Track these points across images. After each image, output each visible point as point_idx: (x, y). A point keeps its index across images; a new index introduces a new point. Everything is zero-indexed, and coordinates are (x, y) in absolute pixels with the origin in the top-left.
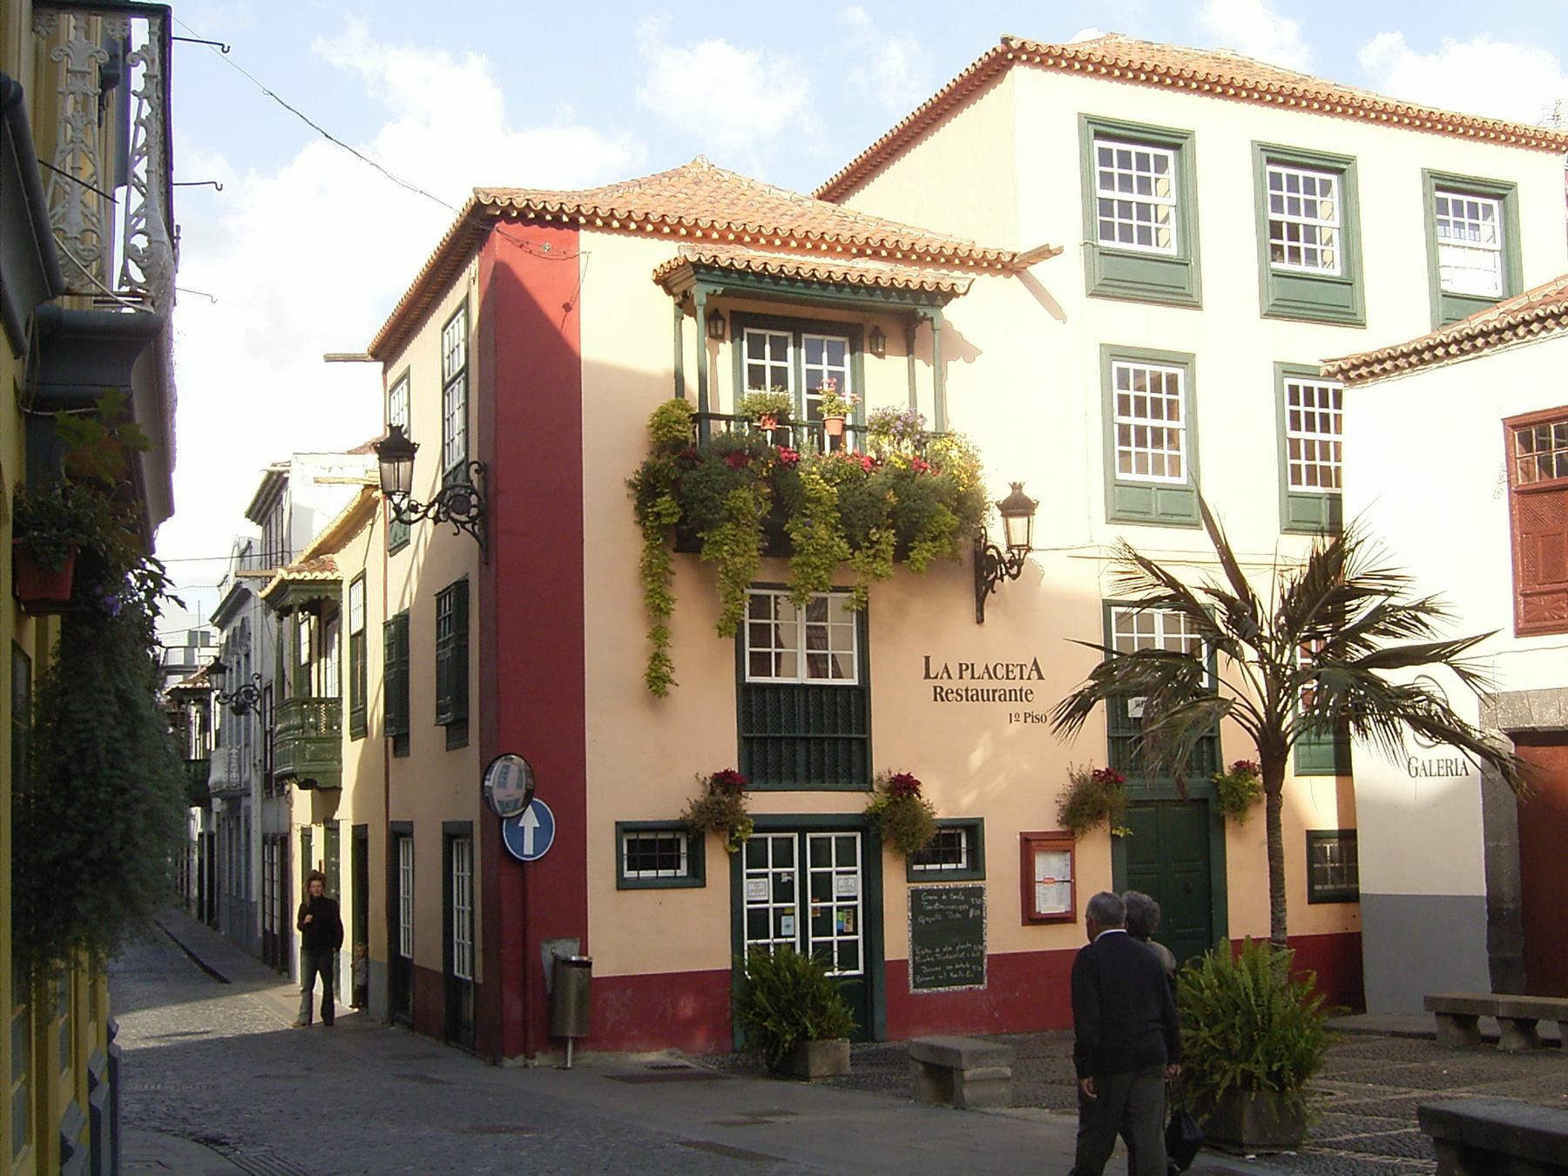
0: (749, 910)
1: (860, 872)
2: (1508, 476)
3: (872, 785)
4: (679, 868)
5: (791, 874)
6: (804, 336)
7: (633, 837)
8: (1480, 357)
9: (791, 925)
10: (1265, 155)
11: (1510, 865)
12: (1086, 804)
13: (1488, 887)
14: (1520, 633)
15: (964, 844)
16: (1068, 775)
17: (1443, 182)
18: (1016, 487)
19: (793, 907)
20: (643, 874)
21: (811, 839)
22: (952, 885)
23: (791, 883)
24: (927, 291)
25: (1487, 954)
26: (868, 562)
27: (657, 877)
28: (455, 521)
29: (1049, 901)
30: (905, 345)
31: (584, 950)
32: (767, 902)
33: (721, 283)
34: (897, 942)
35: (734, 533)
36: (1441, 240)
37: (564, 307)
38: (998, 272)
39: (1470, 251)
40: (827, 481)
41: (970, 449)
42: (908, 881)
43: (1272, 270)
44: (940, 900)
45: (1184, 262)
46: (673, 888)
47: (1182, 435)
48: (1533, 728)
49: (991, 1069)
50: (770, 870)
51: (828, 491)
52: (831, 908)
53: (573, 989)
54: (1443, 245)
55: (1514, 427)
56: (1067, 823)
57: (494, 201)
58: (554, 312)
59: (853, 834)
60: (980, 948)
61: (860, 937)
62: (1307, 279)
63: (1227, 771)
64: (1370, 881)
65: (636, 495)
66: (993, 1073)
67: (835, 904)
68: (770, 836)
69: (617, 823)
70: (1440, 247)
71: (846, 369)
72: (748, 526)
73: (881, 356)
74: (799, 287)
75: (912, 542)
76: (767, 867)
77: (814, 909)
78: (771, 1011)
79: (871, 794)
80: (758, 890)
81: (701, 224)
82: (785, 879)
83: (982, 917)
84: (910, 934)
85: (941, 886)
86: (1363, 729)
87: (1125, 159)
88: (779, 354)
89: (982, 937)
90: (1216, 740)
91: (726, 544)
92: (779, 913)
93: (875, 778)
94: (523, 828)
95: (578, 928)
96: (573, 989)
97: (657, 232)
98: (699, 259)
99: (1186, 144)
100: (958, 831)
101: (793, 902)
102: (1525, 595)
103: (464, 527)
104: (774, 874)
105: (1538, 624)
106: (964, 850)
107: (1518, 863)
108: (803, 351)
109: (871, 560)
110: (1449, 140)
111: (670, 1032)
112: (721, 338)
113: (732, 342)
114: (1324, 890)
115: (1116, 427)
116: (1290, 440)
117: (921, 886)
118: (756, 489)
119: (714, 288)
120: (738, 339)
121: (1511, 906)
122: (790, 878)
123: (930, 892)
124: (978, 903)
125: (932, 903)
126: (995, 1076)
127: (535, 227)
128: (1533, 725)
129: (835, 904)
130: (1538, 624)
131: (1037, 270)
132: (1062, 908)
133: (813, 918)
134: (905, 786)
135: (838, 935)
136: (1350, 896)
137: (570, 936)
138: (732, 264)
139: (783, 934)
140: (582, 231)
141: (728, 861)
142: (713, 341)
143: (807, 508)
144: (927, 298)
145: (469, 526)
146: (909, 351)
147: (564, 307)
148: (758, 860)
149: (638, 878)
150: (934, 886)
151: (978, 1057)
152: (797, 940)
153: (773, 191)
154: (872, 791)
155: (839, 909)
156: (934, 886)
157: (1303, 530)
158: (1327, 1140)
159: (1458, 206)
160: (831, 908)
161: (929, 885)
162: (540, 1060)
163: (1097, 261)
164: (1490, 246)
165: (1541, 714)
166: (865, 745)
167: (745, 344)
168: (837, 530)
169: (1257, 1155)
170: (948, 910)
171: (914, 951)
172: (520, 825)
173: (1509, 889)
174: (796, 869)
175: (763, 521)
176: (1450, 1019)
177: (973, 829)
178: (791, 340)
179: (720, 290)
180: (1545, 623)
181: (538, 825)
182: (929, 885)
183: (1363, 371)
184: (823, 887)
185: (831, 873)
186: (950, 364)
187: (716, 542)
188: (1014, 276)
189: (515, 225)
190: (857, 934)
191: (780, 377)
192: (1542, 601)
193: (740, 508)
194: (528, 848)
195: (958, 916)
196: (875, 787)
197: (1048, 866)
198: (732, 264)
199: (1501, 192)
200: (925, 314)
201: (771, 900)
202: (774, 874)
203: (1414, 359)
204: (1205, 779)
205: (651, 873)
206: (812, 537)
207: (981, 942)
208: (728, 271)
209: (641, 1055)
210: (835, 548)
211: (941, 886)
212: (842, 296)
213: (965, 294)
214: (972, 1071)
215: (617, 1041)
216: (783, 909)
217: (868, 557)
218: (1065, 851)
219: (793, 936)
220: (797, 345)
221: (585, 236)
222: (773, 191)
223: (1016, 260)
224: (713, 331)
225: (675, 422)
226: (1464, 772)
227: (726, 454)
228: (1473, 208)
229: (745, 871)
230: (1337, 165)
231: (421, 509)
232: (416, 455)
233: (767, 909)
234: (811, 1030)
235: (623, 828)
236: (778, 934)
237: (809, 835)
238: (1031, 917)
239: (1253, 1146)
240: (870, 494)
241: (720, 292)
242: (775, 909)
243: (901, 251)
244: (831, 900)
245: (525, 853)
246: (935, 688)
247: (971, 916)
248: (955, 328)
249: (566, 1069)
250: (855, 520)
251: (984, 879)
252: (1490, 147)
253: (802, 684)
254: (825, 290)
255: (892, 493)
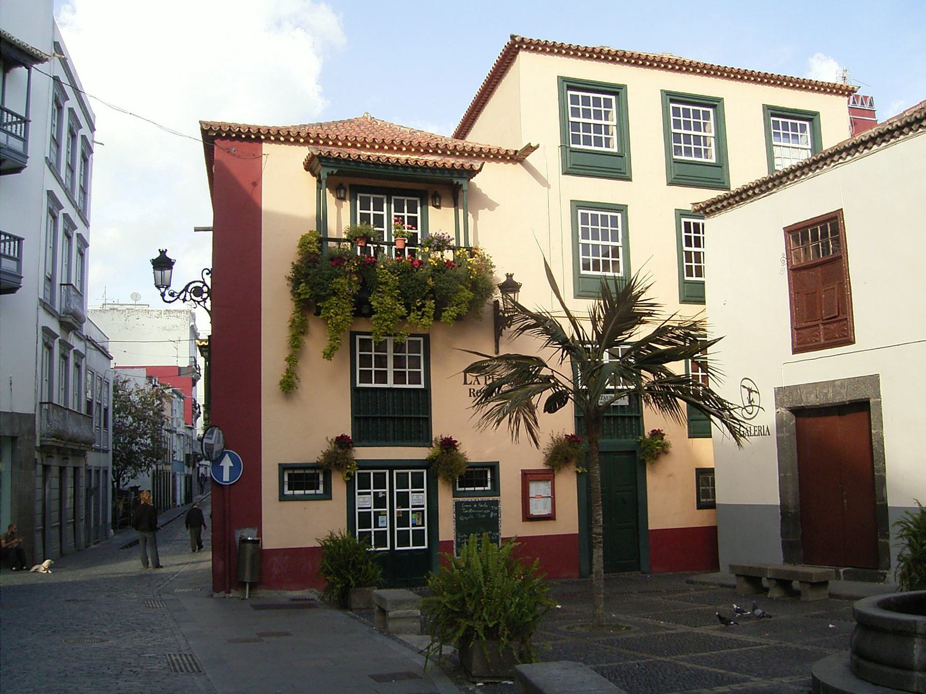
0: (359, 513)
1: (425, 492)
2: (787, 261)
3: (432, 443)
4: (318, 489)
5: (385, 493)
6: (393, 198)
7: (291, 472)
8: (772, 193)
9: (384, 522)
10: (668, 97)
11: (793, 488)
12: (559, 453)
13: (781, 500)
14: (795, 351)
15: (489, 476)
16: (550, 438)
17: (772, 112)
18: (509, 276)
19: (386, 511)
20: (297, 492)
21: (397, 473)
22: (480, 499)
23: (385, 497)
24: (456, 169)
25: (781, 539)
26: (417, 319)
27: (305, 494)
28: (195, 301)
29: (539, 508)
30: (453, 200)
31: (260, 534)
32: (370, 508)
33: (336, 167)
34: (447, 530)
35: (337, 302)
36: (774, 143)
37: (253, 184)
38: (508, 161)
39: (793, 149)
40: (392, 273)
41: (486, 256)
42: (454, 497)
43: (674, 159)
44: (472, 508)
45: (623, 155)
46: (318, 500)
47: (620, 250)
48: (802, 406)
49: (407, 611)
50: (372, 490)
51: (393, 278)
52: (408, 511)
53: (248, 555)
54: (777, 146)
55: (789, 232)
56: (550, 465)
57: (211, 128)
58: (247, 186)
59: (422, 470)
60: (497, 534)
61: (426, 528)
62: (700, 165)
63: (647, 435)
64: (721, 498)
65: (292, 285)
66: (408, 614)
67: (410, 509)
68: (372, 472)
69: (279, 464)
70: (774, 147)
71: (419, 215)
72: (345, 299)
73: (438, 207)
74: (381, 168)
75: (445, 307)
76: (370, 489)
77: (398, 512)
78: (332, 570)
79: (431, 448)
80: (365, 502)
81: (330, 137)
82: (381, 495)
83: (498, 517)
84: (455, 526)
85: (473, 499)
86: (647, 401)
87: (586, 101)
88: (378, 207)
89: (498, 528)
90: (641, 418)
91: (332, 309)
92: (377, 514)
93: (433, 439)
94: (223, 467)
95: (256, 520)
96: (248, 555)
97: (297, 142)
98: (320, 153)
99: (622, 92)
100: (485, 469)
101: (386, 508)
102: (796, 329)
103: (199, 304)
104: (374, 493)
105: (804, 346)
106: (489, 480)
107: (798, 485)
108: (393, 206)
109: (419, 317)
110: (778, 89)
111: (302, 581)
112: (344, 199)
113: (350, 201)
114: (707, 502)
115: (580, 245)
116: (685, 251)
117: (461, 499)
118: (350, 279)
119: (331, 170)
120: (353, 200)
121: (793, 511)
122: (384, 495)
123: (467, 503)
124: (496, 509)
125: (469, 508)
126: (409, 615)
127: (237, 142)
128: (803, 405)
129: (410, 509)
130: (804, 346)
131: (530, 159)
132: (547, 511)
133: (398, 518)
134: (449, 445)
135: (413, 526)
136: (712, 506)
137: (251, 526)
138: (339, 156)
139: (380, 526)
140: (264, 144)
141: (345, 485)
142: (339, 201)
143: (380, 288)
144: (458, 174)
145: (202, 303)
146: (456, 205)
147: (253, 184)
148: (364, 484)
149: (293, 494)
150: (469, 499)
151: (398, 603)
152: (388, 529)
153: (401, 128)
154: (432, 447)
155: (413, 512)
156: (469, 499)
157: (694, 302)
158: (601, 665)
159: (785, 125)
160: (408, 511)
161: (466, 499)
162: (234, 593)
163: (568, 155)
164: (805, 146)
165: (807, 399)
166: (428, 421)
167: (358, 202)
168: (399, 300)
169: (485, 683)
170: (477, 513)
171: (457, 535)
172: (221, 465)
173: (792, 501)
174: (387, 490)
175: (354, 296)
176: (742, 579)
177: (494, 467)
178: (385, 200)
179: (335, 171)
180: (807, 345)
181: (232, 465)
182: (466, 499)
183: (713, 208)
184: (403, 500)
185: (408, 492)
186: (480, 211)
187: (326, 308)
188: (518, 164)
189: (225, 141)
190: (424, 526)
191: (379, 220)
192: (804, 332)
193: (339, 289)
194: (226, 477)
195: (484, 516)
196: (434, 445)
197: (538, 489)
198: (339, 156)
199: (810, 117)
200: (458, 182)
201: (372, 507)
202: (374, 493)
203: (737, 199)
204: (634, 440)
205: (302, 492)
206: (382, 304)
207: (498, 530)
208: (338, 160)
209: (293, 592)
210: (397, 310)
211: (473, 499)
212: (407, 173)
213: (480, 170)
214: (394, 612)
215: (279, 583)
216: (380, 512)
217: (418, 315)
218: (548, 480)
219: (386, 527)
220: (389, 203)
221: (266, 147)
222: (401, 128)
223: (518, 154)
224: (339, 196)
225: (308, 243)
226: (767, 434)
227: (332, 259)
228: (794, 127)
229: (357, 491)
230: (711, 103)
231: (176, 295)
232: (173, 267)
233: (370, 512)
234: (353, 582)
235: (283, 468)
236: (376, 526)
237: (395, 472)
238: (528, 517)
239: (481, 678)
240: (417, 280)
241: (335, 172)
242: (375, 512)
243: (450, 150)
244: (409, 508)
245: (224, 480)
246: (470, 389)
247: (491, 516)
248: (483, 192)
249: (243, 599)
250: (408, 294)
251: (499, 496)
252: (803, 93)
253: (391, 388)
254: (406, 170)
255: (431, 280)
